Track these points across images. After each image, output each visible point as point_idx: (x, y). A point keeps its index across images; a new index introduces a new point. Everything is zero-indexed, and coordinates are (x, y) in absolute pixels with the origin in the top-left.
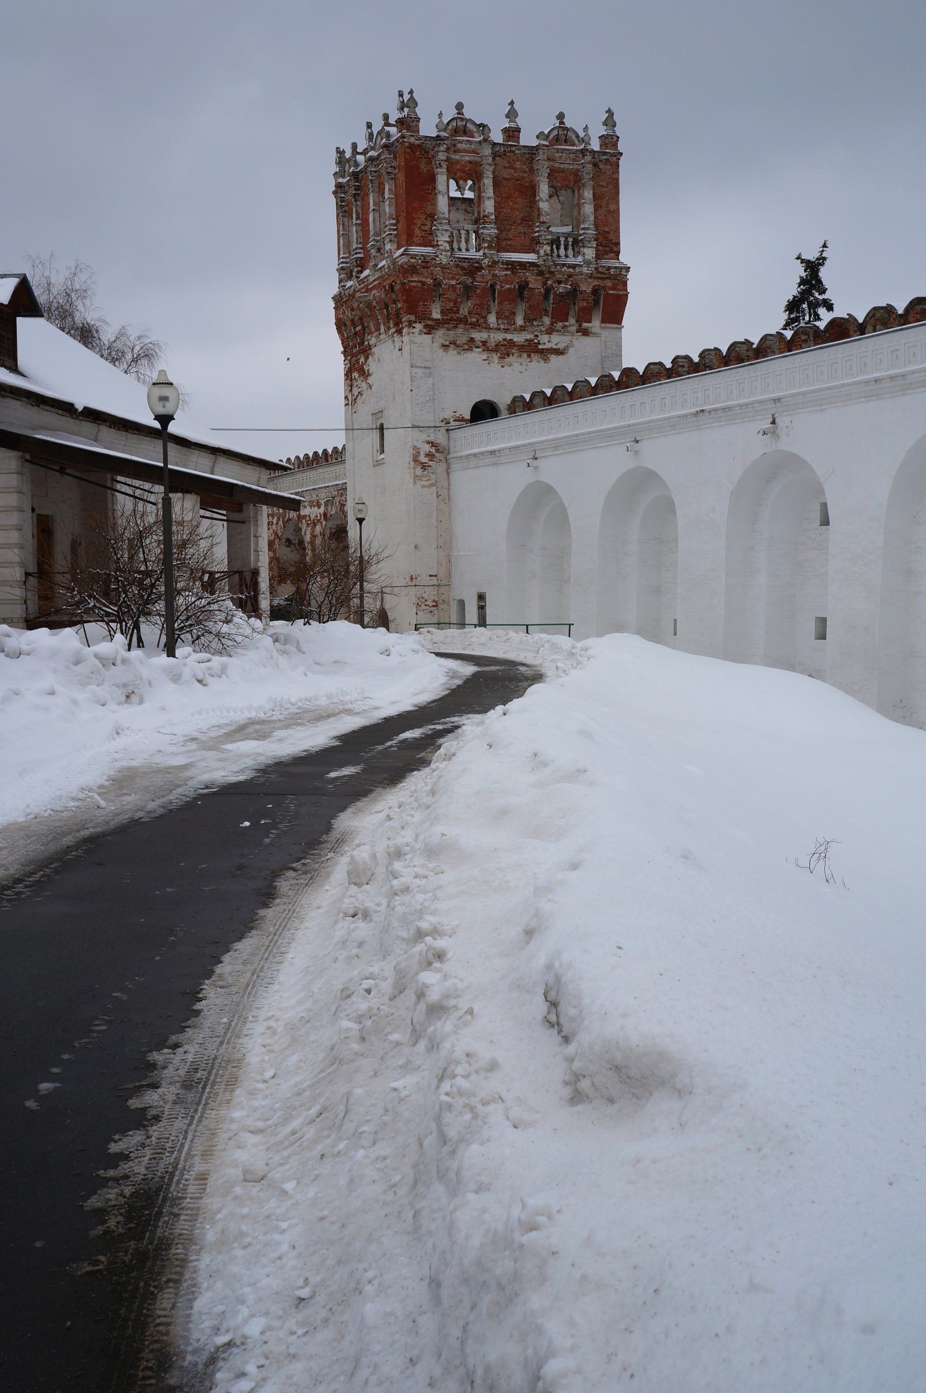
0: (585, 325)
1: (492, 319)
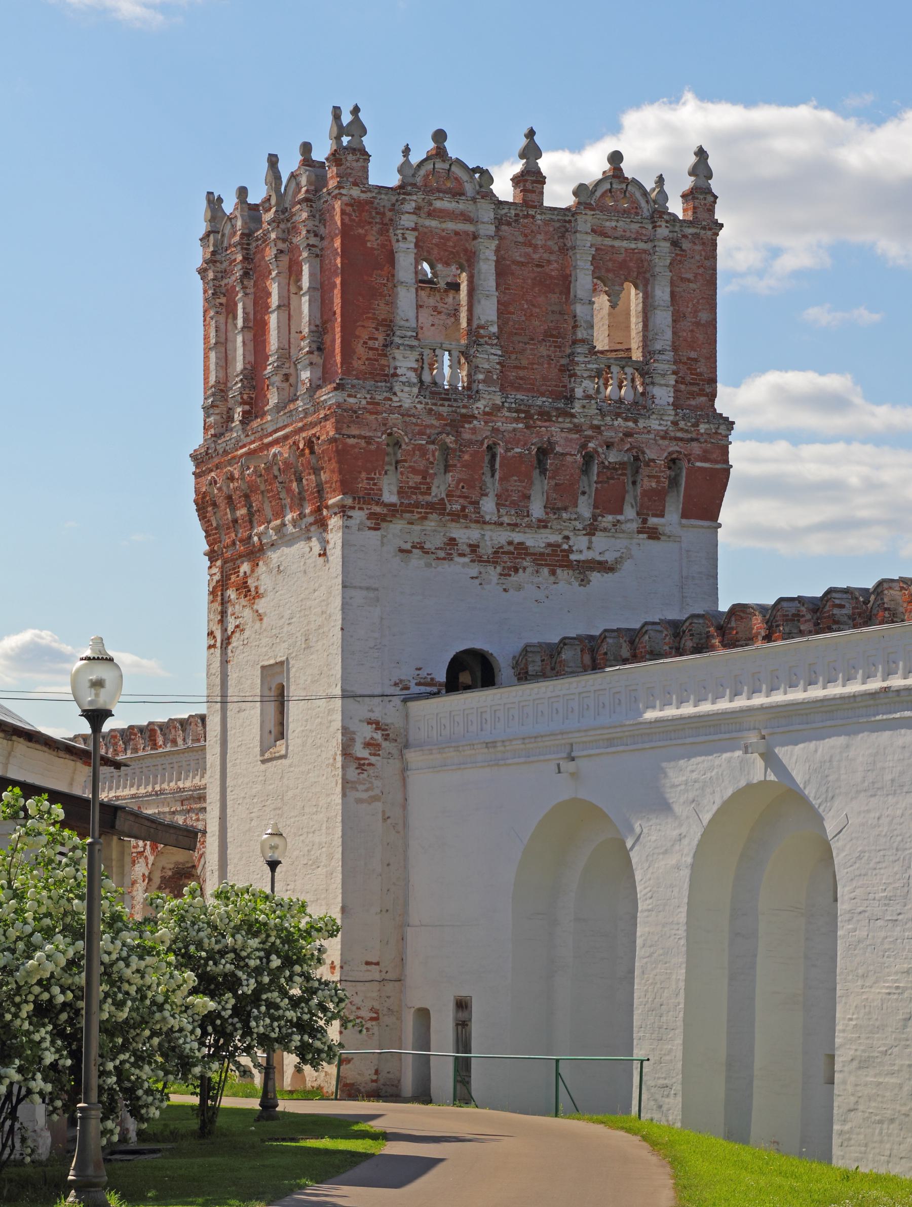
0: (653, 521)
1: (488, 505)
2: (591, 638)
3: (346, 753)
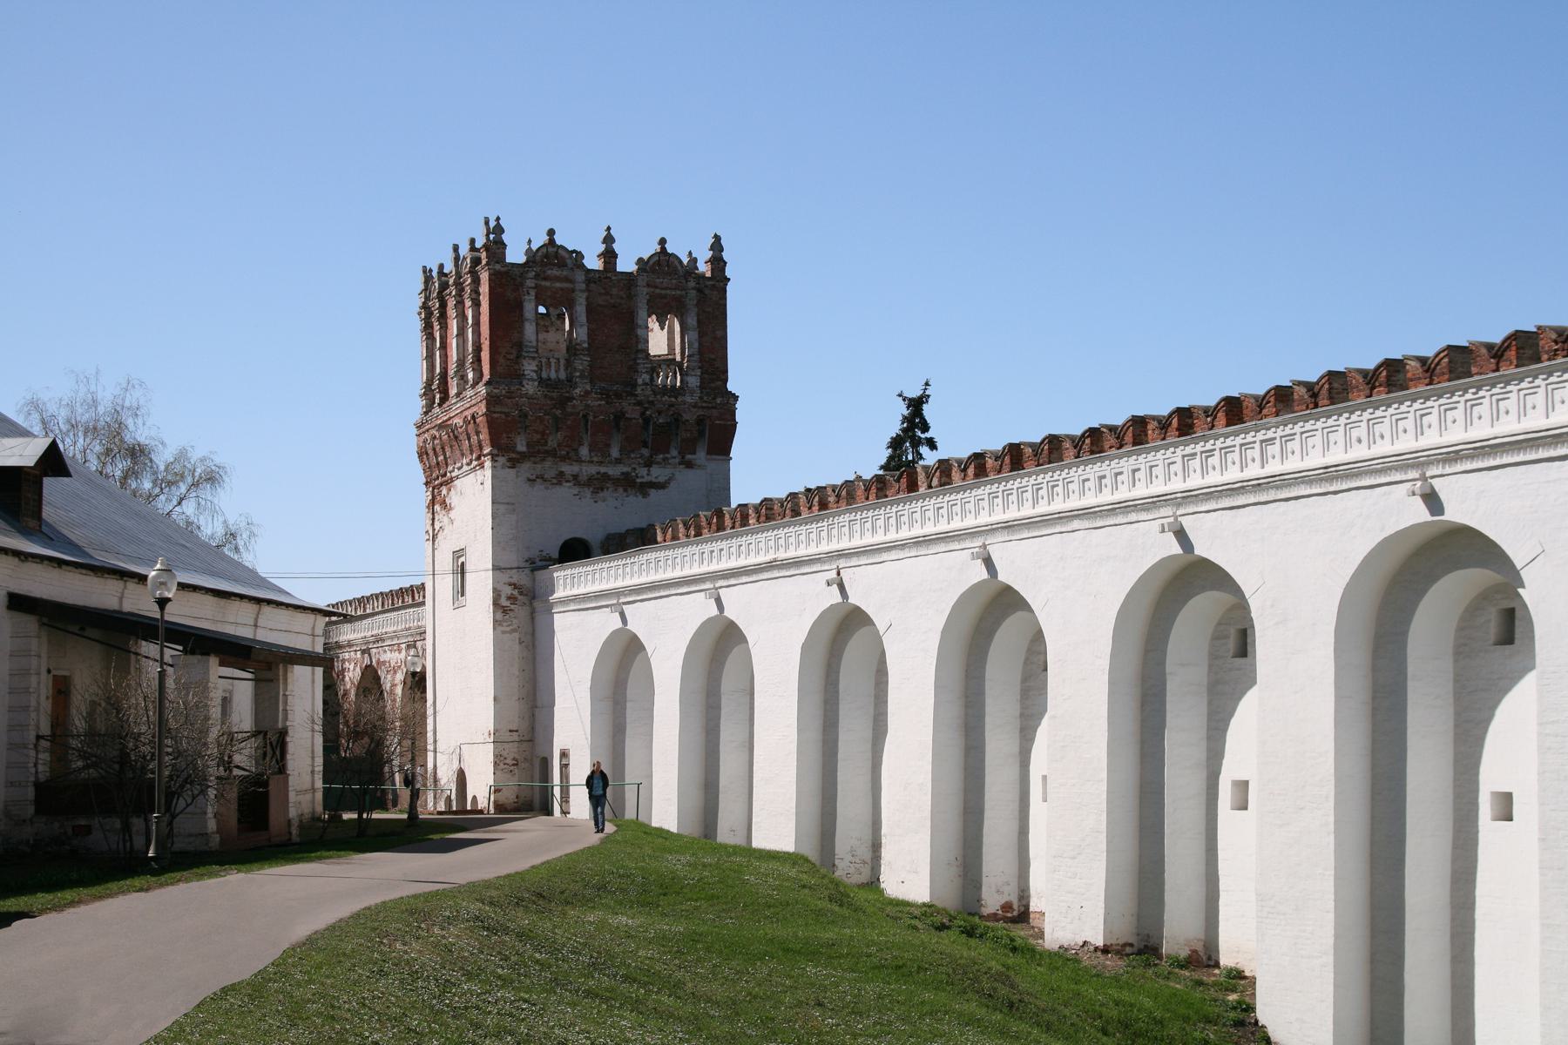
0: (689, 457)
1: (584, 451)
2: (642, 530)
3: (496, 603)
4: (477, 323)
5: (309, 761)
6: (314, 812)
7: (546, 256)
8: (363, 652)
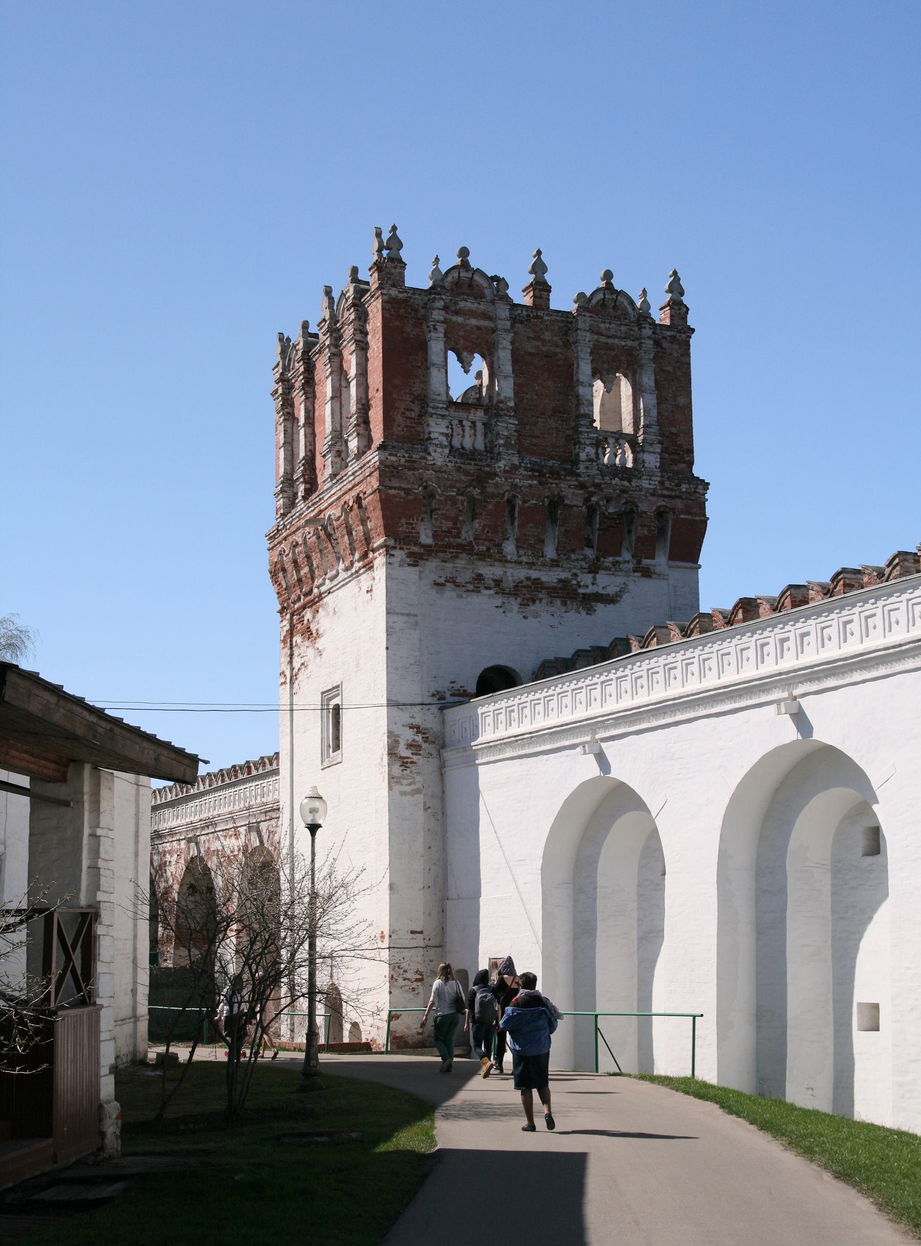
0: (646, 562)
1: (509, 548)
3: (392, 753)
4: (363, 373)
5: (129, 976)
6: (135, 1052)
7: (457, 283)
8: (189, 840)
